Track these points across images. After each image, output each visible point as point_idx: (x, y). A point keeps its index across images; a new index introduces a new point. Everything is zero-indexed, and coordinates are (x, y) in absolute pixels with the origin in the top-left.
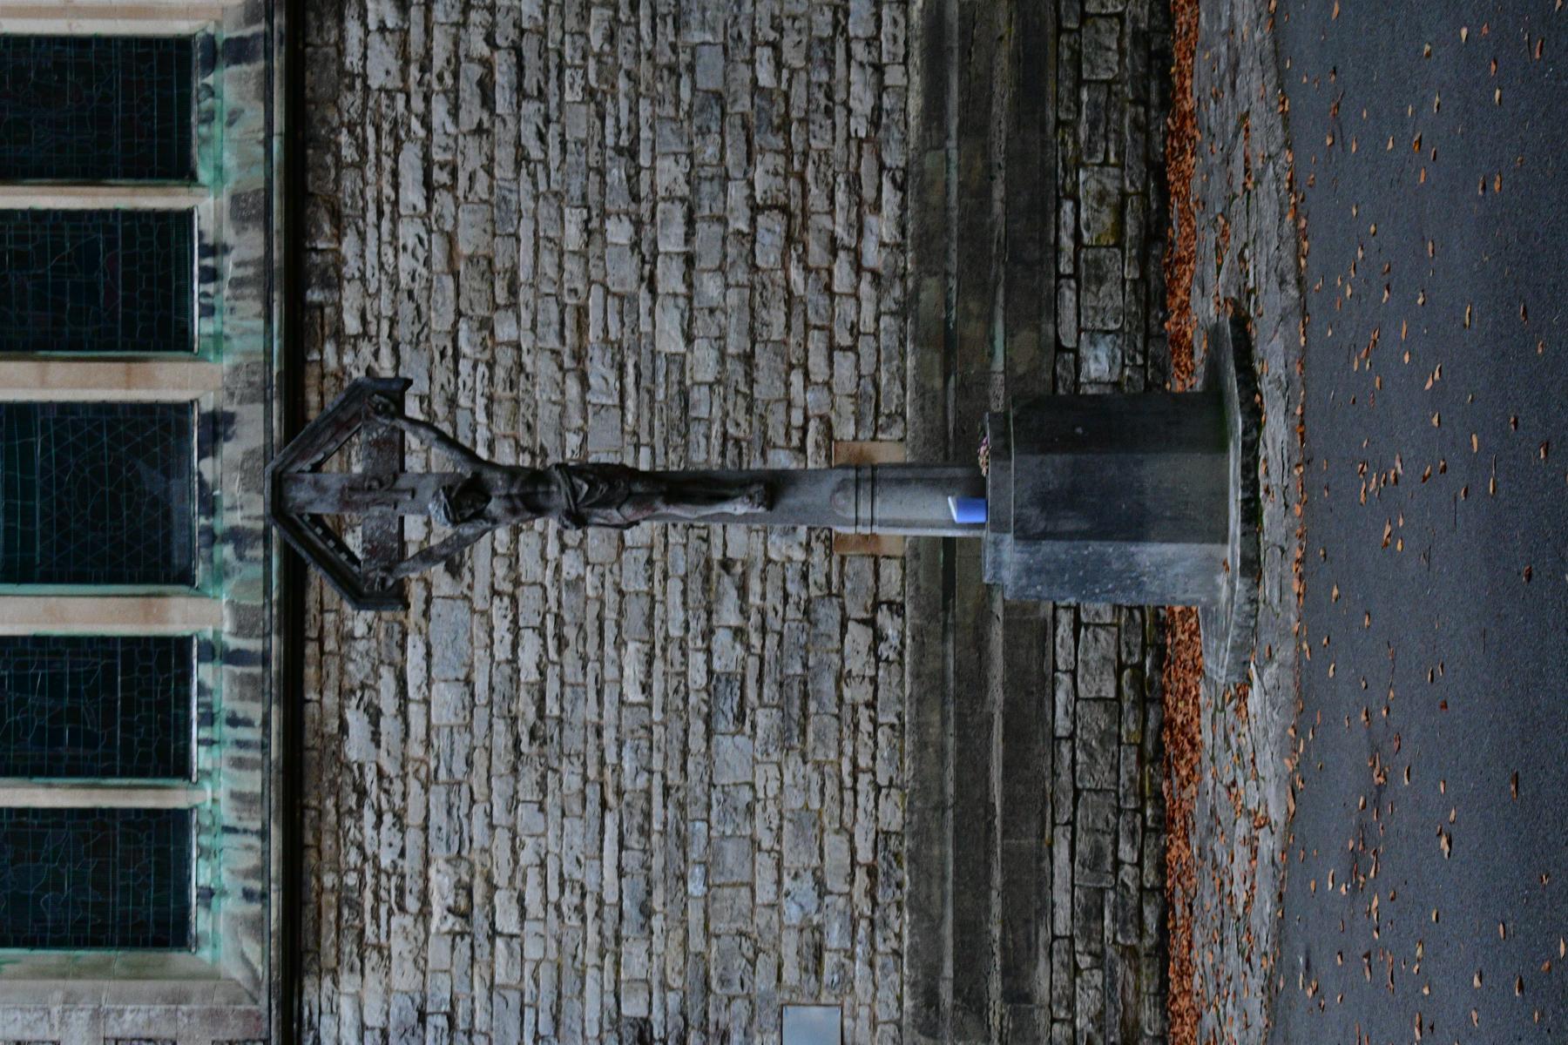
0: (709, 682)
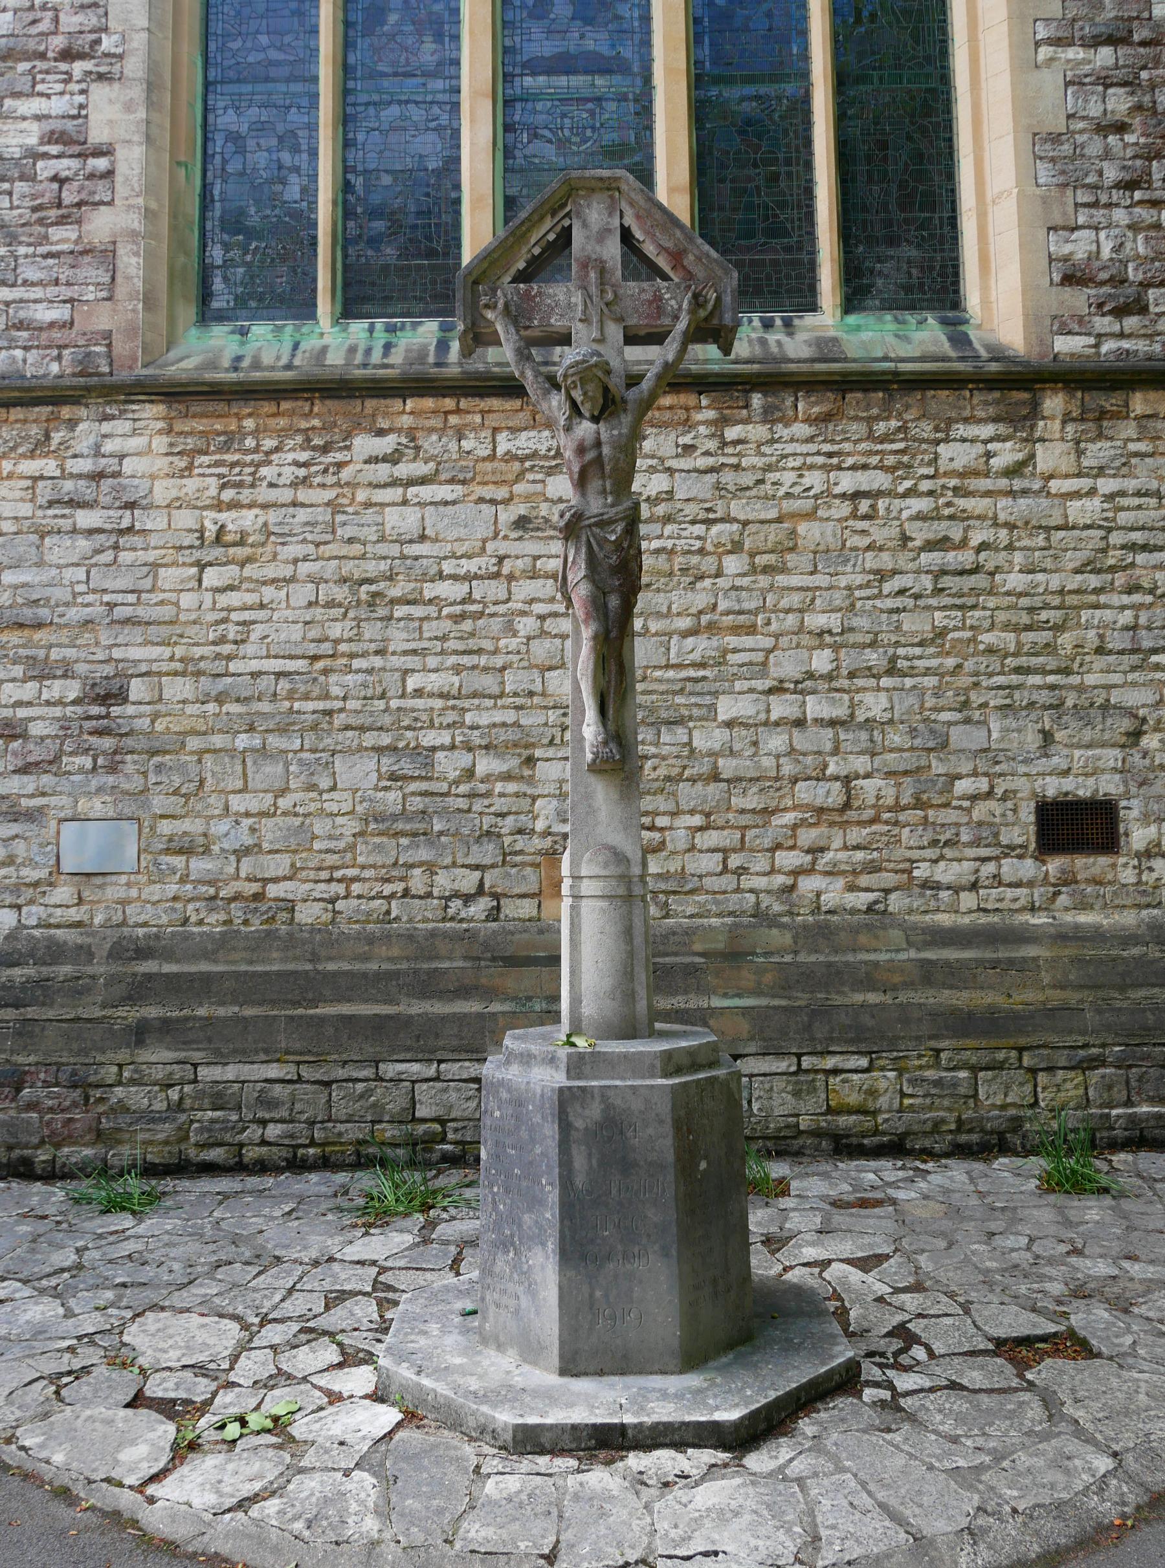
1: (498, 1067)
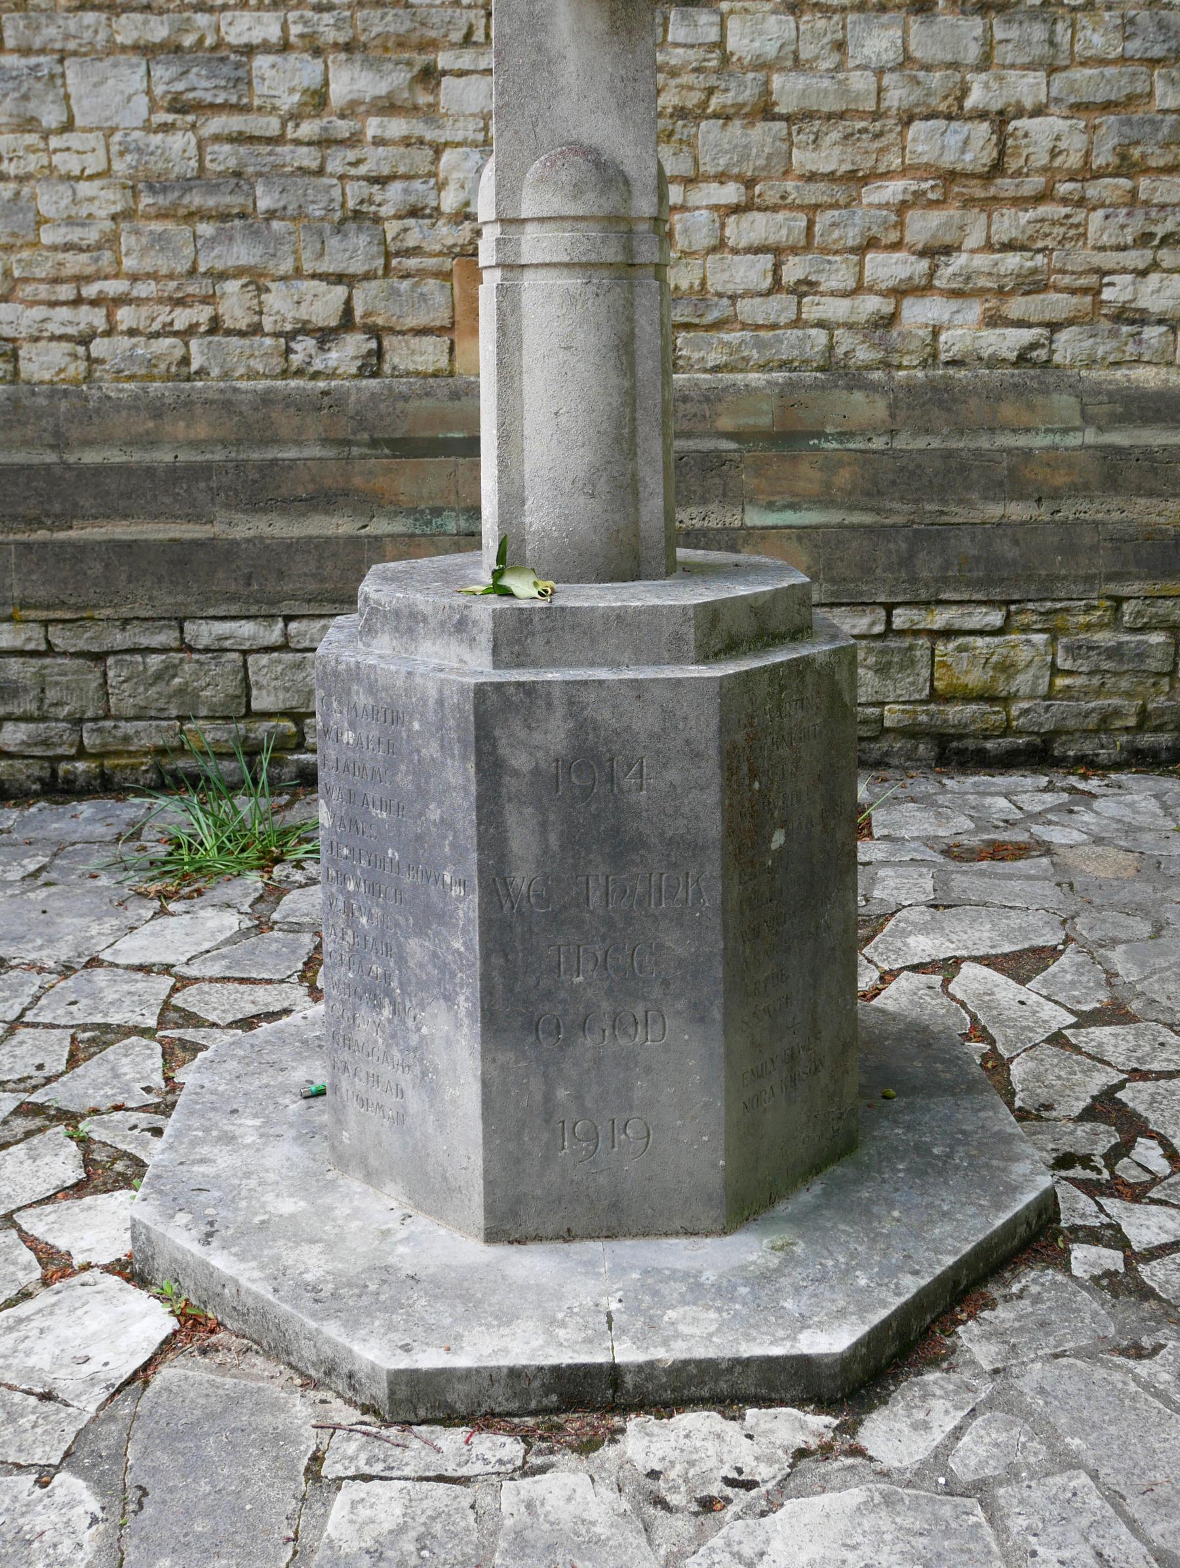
0: (236, 49)
1: (352, 639)
